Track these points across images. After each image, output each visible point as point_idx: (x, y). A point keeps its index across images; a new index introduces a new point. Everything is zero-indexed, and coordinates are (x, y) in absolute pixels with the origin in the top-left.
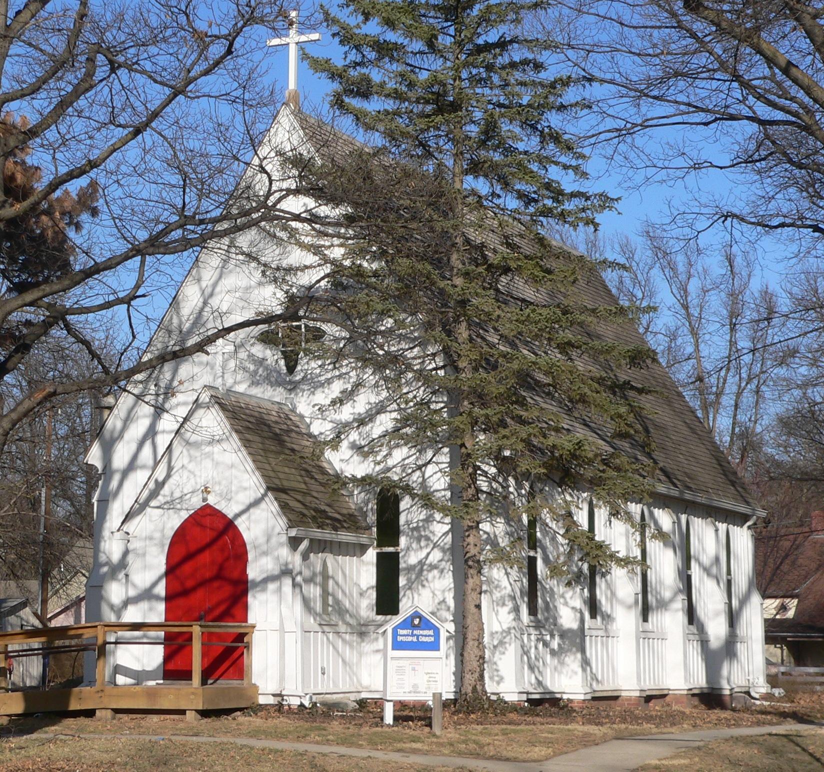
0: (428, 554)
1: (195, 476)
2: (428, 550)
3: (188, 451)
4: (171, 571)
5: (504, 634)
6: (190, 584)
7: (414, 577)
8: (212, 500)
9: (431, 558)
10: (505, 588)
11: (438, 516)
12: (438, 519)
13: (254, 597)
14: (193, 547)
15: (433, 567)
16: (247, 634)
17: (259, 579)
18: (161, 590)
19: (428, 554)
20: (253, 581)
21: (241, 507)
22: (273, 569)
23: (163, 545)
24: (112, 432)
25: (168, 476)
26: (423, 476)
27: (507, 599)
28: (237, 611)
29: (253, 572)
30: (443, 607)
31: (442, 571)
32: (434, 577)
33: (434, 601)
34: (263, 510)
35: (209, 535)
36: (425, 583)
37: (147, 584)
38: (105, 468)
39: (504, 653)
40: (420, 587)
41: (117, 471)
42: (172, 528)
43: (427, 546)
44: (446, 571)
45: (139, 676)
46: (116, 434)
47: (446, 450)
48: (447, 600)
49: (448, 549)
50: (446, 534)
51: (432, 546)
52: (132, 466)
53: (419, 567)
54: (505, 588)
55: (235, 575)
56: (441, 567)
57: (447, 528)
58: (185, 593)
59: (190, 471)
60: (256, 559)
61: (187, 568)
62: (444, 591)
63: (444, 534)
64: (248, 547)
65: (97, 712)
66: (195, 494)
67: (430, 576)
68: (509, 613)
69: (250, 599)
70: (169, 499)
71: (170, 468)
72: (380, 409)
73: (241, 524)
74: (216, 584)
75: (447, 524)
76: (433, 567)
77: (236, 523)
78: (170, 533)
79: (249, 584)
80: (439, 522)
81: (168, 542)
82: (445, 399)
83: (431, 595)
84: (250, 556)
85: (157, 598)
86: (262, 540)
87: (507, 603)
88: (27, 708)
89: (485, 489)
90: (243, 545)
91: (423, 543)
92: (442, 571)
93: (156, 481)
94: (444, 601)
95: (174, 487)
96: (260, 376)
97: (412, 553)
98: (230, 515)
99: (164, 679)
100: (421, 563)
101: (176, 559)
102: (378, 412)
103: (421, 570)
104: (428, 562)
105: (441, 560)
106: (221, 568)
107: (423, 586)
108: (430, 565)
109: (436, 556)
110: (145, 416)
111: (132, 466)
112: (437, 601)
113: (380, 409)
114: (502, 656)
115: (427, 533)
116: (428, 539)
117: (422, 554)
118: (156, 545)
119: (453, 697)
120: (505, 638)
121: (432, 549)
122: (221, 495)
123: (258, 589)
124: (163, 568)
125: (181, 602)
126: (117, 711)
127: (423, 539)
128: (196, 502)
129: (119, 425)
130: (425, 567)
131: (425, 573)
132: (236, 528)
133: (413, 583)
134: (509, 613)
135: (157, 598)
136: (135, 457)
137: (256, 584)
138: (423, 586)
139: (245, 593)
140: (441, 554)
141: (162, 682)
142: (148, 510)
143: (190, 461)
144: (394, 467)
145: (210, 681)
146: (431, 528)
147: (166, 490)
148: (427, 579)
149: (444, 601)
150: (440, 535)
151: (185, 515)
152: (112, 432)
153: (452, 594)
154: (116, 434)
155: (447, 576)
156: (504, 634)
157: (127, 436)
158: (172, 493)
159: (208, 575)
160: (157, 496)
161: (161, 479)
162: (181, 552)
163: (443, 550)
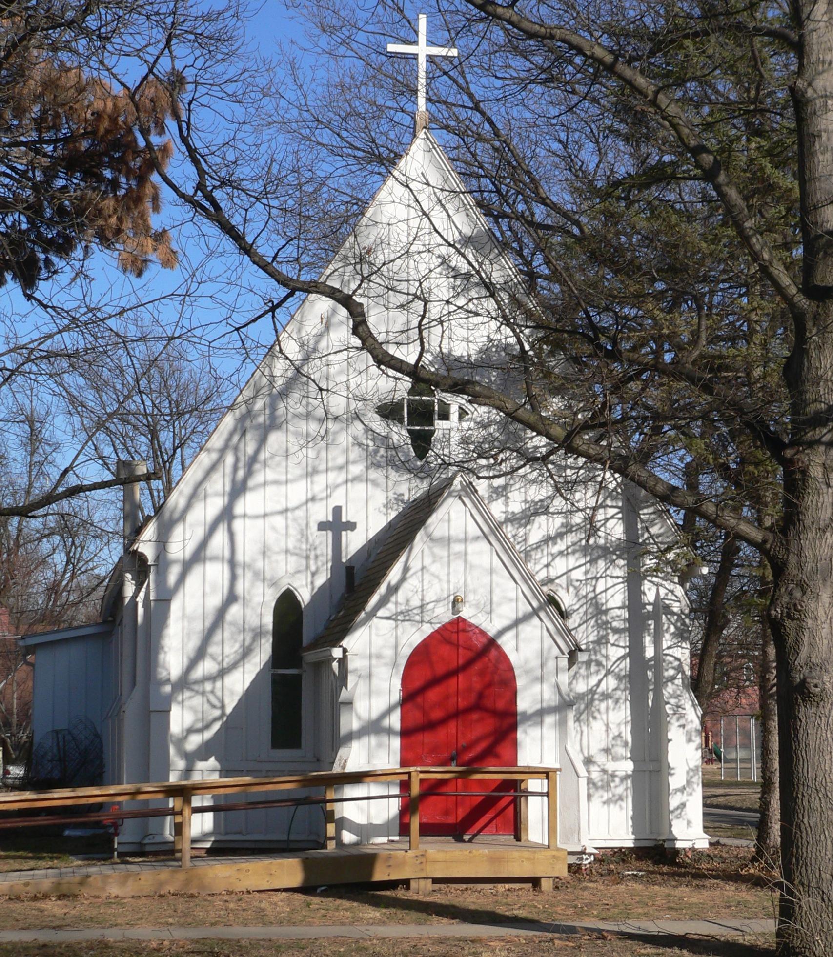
0: (600, 681)
1: (440, 580)
2: (600, 677)
3: (430, 548)
4: (409, 698)
5: (691, 774)
6: (437, 714)
7: (582, 707)
8: (466, 613)
9: (603, 686)
10: (692, 722)
11: (612, 638)
12: (612, 642)
13: (526, 732)
14: (440, 670)
15: (606, 696)
16: (522, 781)
17: (530, 711)
18: (395, 721)
19: (600, 681)
20: (524, 713)
21: (506, 623)
22: (550, 699)
23: (395, 665)
24: (172, 512)
25: (403, 579)
26: (594, 591)
27: (694, 734)
28: (504, 750)
29: (525, 703)
30: (619, 743)
31: (617, 701)
32: (607, 709)
33: (608, 735)
34: (535, 627)
35: (463, 656)
36: (596, 714)
37: (375, 715)
38: (157, 558)
39: (691, 794)
40: (591, 719)
41: (175, 562)
42: (411, 645)
43: (597, 672)
44: (621, 701)
45: (365, 831)
46: (176, 515)
47: (621, 562)
48: (623, 735)
49: (624, 676)
50: (622, 658)
51: (603, 672)
52: (199, 556)
53: (590, 696)
54: (692, 722)
55: (501, 705)
56: (617, 696)
57: (621, 652)
58: (430, 726)
59: (433, 574)
60: (525, 688)
61: (433, 695)
62: (619, 725)
63: (619, 659)
64: (517, 672)
65: (543, 880)
66: (441, 604)
67: (603, 706)
68: (697, 749)
69: (520, 734)
70: (402, 608)
71: (406, 569)
72: (540, 509)
73: (507, 643)
74: (475, 716)
75: (624, 647)
76: (606, 696)
77: (500, 642)
78: (406, 651)
79: (519, 718)
80: (613, 645)
81: (403, 662)
82: (620, 504)
83: (604, 728)
84: (520, 683)
85: (389, 731)
86: (535, 663)
87: (693, 738)
88: (306, 879)
89: (676, 610)
90: (511, 669)
91: (593, 668)
92: (617, 701)
93: (389, 584)
94: (619, 736)
95: (411, 594)
96: (382, 456)
97: (580, 680)
98: (491, 633)
99: (400, 835)
100: (592, 691)
101: (418, 684)
102: (536, 514)
103: (592, 700)
104: (600, 690)
105: (616, 689)
106: (481, 695)
107: (595, 718)
108: (603, 694)
109: (611, 683)
110: (216, 494)
111: (199, 556)
112: (611, 736)
113: (540, 509)
114: (690, 798)
115: (599, 657)
116: (599, 664)
117: (593, 681)
118: (386, 665)
119: (632, 845)
120: (692, 777)
121: (605, 675)
122: (477, 606)
123: (530, 723)
124: (396, 695)
125: (428, 738)
126: (436, 881)
127: (593, 664)
128: (443, 614)
129: (182, 503)
130: (596, 696)
131: (597, 703)
132: (499, 648)
133: (581, 714)
134: (697, 749)
135: (389, 731)
136: (203, 545)
137: (527, 717)
138: (595, 718)
139: (513, 728)
140: (616, 682)
141: (397, 838)
142: (375, 620)
143: (434, 562)
144: (558, 578)
145: (466, 837)
146: (604, 651)
147: (401, 596)
148: (599, 710)
149: (619, 736)
150: (614, 659)
151: (428, 630)
152: (172, 512)
153: (629, 728)
154: (176, 515)
155: (623, 707)
156: (691, 774)
157: (191, 517)
158: (408, 601)
159: (462, 704)
160: (387, 603)
161: (393, 583)
162: (421, 676)
163: (619, 678)
